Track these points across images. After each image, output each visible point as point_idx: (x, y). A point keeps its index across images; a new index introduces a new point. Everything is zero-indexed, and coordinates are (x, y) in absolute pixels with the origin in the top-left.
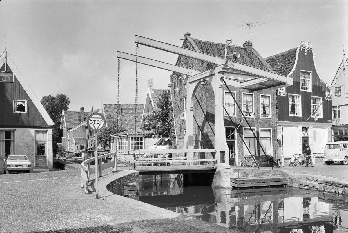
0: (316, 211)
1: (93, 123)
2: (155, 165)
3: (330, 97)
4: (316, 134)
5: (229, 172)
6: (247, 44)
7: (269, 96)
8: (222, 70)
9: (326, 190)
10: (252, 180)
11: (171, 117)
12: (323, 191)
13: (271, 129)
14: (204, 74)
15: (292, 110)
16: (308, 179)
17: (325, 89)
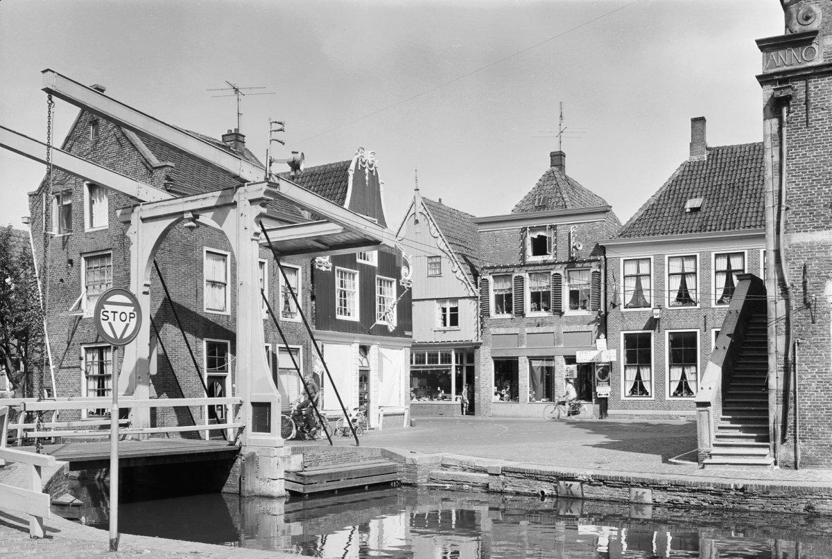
0: (380, 539)
1: (111, 320)
2: (26, 441)
3: (409, 281)
4: (384, 358)
5: (282, 455)
6: (234, 137)
7: (298, 269)
8: (264, 196)
9: (509, 489)
10: (336, 473)
11: (32, 308)
12: (502, 492)
13: (300, 347)
15: (341, 305)
16: (445, 466)
17: (400, 263)
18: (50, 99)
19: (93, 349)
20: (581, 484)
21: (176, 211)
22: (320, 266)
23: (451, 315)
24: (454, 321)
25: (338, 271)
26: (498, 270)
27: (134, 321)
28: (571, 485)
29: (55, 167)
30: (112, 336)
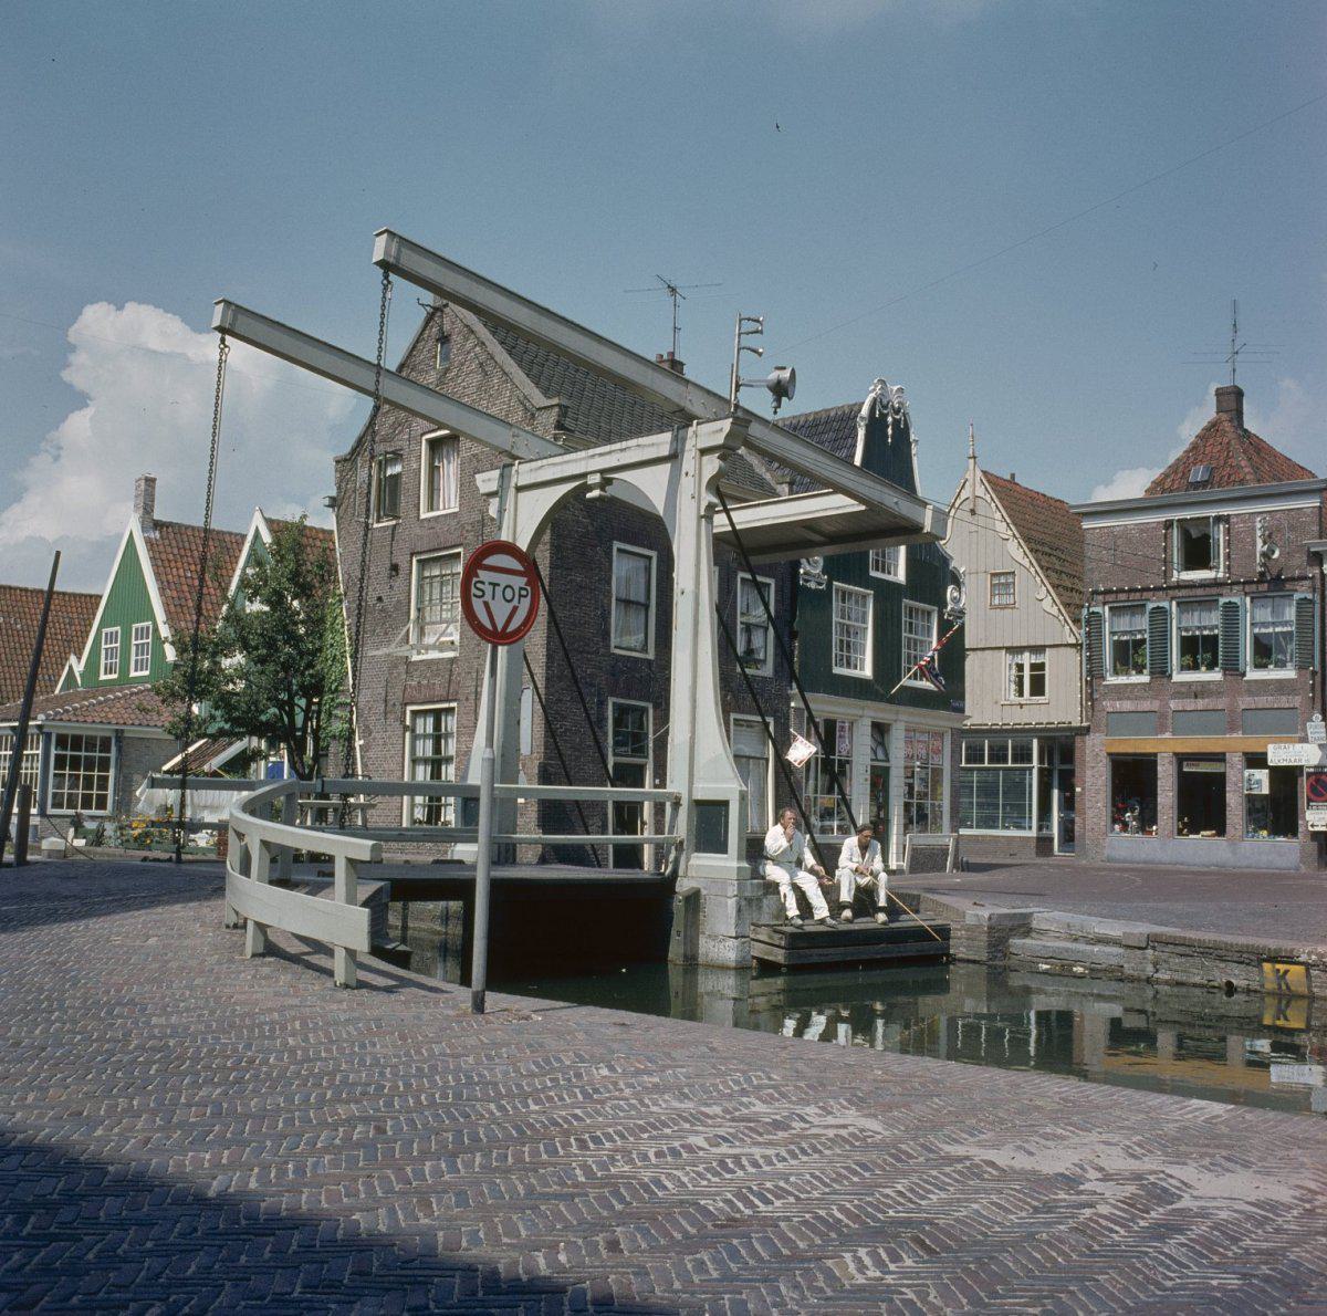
1: (488, 597)
12: (1148, 980)
14: (610, 452)
18: (386, 277)
19: (425, 713)
20: (1307, 971)
21: (575, 473)
22: (807, 581)
23: (1031, 675)
24: (1038, 687)
25: (837, 590)
26: (1122, 597)
27: (526, 603)
28: (1286, 972)
29: (387, 401)
30: (489, 626)
